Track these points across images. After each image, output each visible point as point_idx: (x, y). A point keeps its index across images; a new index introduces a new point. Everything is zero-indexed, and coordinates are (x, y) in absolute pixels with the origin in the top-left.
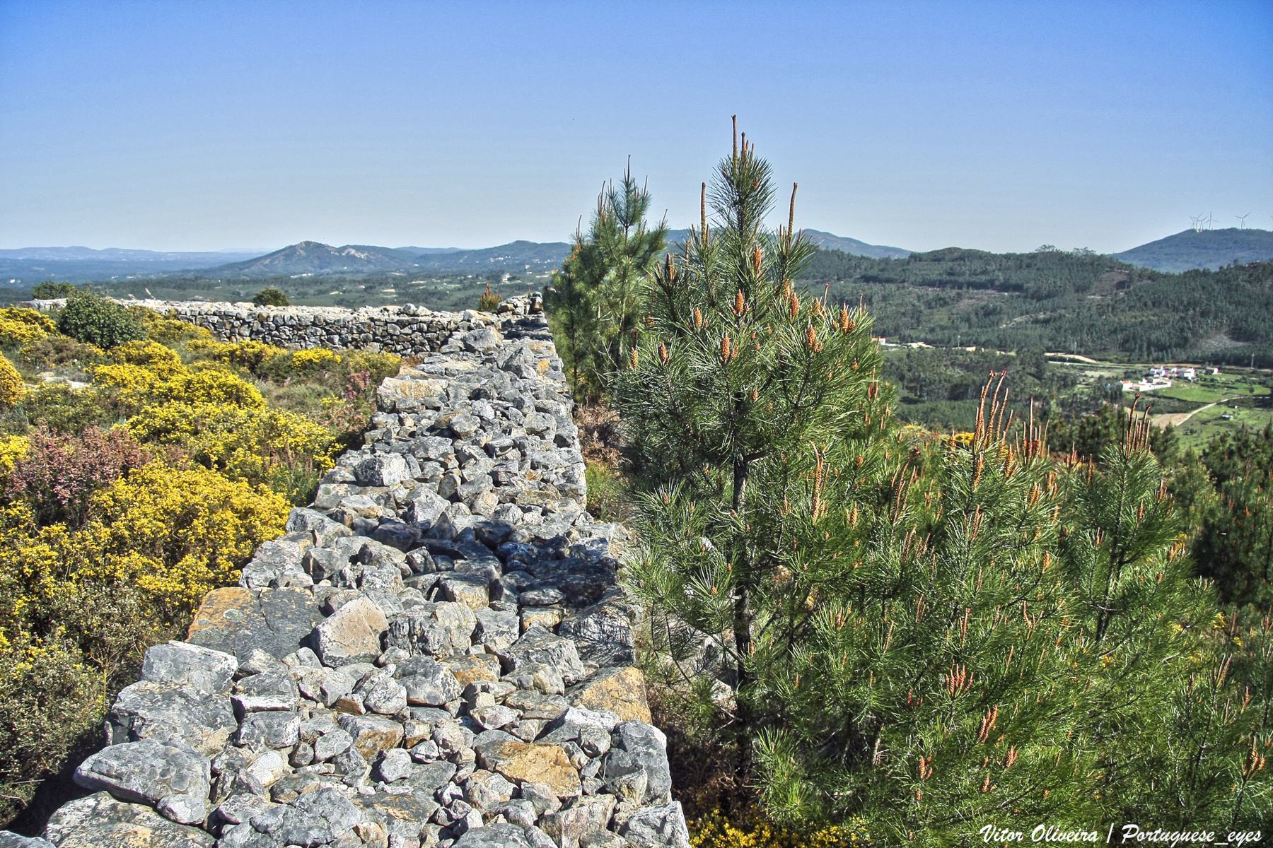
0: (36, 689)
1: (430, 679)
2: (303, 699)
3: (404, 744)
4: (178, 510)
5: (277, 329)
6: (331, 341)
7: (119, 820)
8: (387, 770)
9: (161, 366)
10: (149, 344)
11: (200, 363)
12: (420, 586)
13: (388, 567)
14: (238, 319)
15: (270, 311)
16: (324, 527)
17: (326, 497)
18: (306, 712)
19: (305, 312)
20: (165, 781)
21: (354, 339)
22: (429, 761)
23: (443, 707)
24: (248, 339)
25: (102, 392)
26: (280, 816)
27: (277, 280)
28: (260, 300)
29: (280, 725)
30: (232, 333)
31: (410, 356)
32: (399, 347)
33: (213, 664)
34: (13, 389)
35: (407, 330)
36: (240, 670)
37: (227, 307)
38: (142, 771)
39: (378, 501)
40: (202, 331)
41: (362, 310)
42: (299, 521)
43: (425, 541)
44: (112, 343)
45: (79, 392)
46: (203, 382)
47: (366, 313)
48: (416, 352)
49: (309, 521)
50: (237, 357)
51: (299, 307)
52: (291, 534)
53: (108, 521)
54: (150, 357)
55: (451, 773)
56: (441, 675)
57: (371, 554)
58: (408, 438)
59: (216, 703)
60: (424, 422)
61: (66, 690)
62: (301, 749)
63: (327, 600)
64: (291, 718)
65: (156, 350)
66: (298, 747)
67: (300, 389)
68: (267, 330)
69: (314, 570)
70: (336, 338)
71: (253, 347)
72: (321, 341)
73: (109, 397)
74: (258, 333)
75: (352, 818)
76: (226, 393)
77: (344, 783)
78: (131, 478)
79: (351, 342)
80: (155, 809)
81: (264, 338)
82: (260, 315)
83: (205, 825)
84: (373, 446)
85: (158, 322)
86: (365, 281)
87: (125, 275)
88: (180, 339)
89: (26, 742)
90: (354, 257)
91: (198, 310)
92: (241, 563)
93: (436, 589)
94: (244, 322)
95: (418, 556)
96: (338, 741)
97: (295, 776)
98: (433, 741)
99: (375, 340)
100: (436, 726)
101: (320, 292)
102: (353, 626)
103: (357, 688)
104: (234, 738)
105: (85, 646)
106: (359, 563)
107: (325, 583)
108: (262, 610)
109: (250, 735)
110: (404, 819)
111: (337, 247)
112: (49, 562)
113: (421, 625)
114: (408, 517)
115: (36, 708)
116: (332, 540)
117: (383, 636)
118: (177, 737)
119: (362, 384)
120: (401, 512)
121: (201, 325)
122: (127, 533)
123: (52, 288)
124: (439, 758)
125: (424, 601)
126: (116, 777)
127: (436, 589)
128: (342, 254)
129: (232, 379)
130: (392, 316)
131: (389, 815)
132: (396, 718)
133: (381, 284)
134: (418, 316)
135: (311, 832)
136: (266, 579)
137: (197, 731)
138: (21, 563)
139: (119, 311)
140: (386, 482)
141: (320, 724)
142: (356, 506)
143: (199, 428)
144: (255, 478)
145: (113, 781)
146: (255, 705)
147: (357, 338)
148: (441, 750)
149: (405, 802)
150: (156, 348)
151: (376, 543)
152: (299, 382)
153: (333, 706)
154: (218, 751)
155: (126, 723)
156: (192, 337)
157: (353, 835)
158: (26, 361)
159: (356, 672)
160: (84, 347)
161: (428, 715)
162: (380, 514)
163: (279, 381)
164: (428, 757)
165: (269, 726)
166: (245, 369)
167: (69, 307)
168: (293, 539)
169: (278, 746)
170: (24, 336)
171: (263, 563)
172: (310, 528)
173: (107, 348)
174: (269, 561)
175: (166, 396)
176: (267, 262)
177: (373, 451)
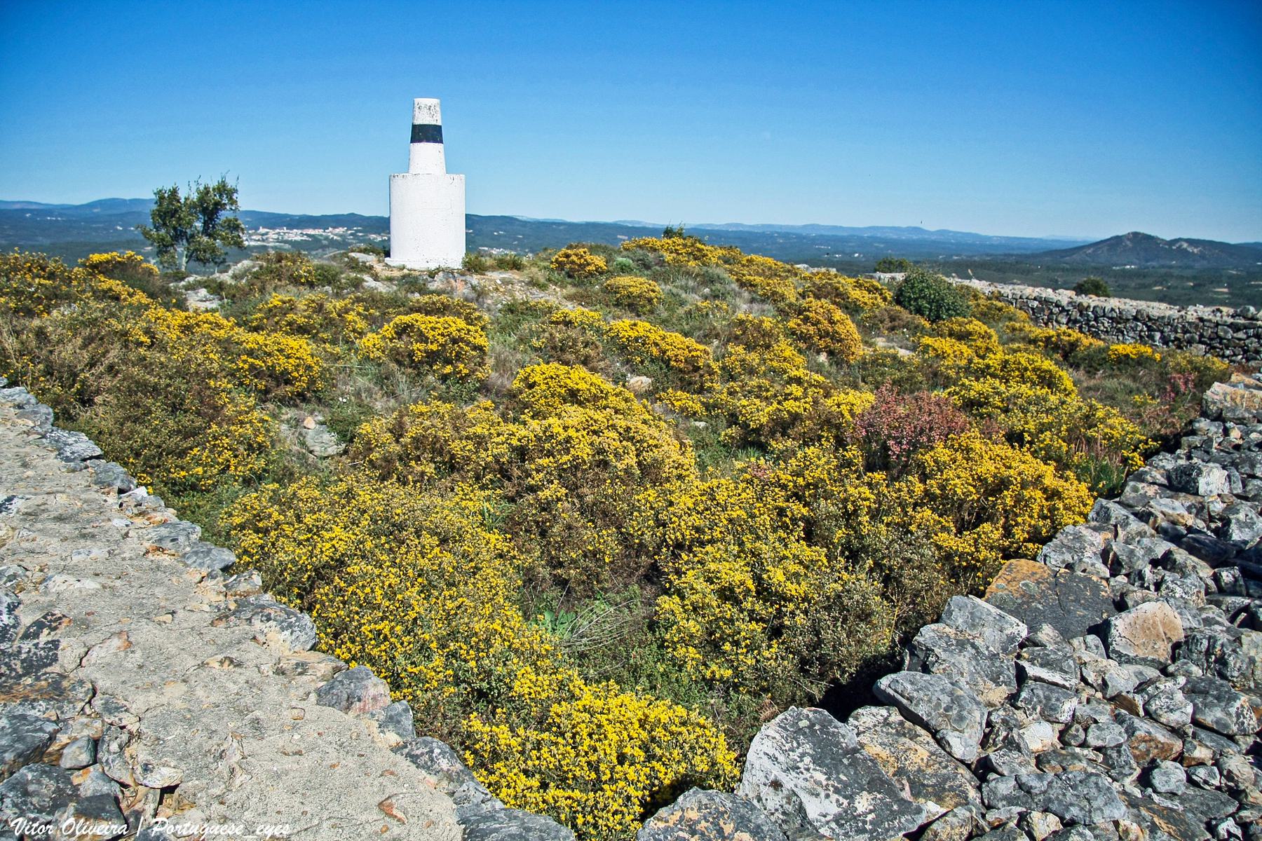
0: (843, 608)
1: (1223, 704)
2: (1083, 684)
3: (1180, 759)
4: (990, 480)
5: (1096, 319)
6: (1151, 337)
7: (904, 735)
8: (1158, 779)
9: (979, 344)
10: (971, 322)
11: (1016, 346)
12: (1224, 607)
13: (1192, 580)
14: (1057, 306)
15: (1091, 301)
16: (1128, 524)
17: (1133, 495)
18: (1084, 696)
19: (1129, 306)
20: (946, 716)
21: (1176, 339)
22: (1207, 787)
23: (1231, 738)
24: (1064, 328)
25: (925, 361)
26: (1045, 783)
27: (1096, 270)
28: (1080, 290)
29: (1058, 700)
30: (1050, 320)
31: (1240, 363)
32: (1228, 352)
33: (1006, 626)
34: (853, 349)
35: (1241, 335)
36: (1028, 639)
37: (1048, 293)
38: (929, 701)
39: (1189, 509)
40: (1021, 315)
41: (1191, 308)
42: (1102, 513)
43: (1239, 562)
44: (938, 317)
45: (906, 359)
46: (1020, 363)
47: (1195, 312)
48: (1248, 360)
49: (1113, 515)
50: (1052, 343)
51: (1123, 300)
52: (1093, 524)
53: (924, 478)
54: (970, 334)
55: (1231, 810)
56: (1238, 704)
57: (1175, 561)
58: (1232, 451)
59: (1002, 662)
60: (1253, 436)
61: (865, 616)
62: (1073, 729)
63: (1123, 595)
64: (1068, 697)
65: (976, 328)
66: (1071, 726)
67: (1112, 383)
68: (1084, 319)
69: (1112, 561)
70: (1158, 335)
71: (1069, 335)
72: (1141, 337)
73: (931, 367)
74: (1075, 321)
75: (1115, 811)
76: (1039, 377)
77: (1110, 776)
78: (949, 443)
79: (1173, 341)
80: (934, 736)
81: (1080, 328)
82: (1080, 304)
83: (973, 766)
84: (1190, 452)
85: (981, 302)
86: (1194, 278)
87: (952, 256)
88: (999, 320)
89: (826, 649)
90: (1185, 250)
91: (1019, 293)
92: (1038, 538)
93: (1243, 615)
94: (1063, 310)
95: (1227, 576)
96: (1113, 735)
97: (1063, 752)
98: (1215, 769)
99: (1201, 342)
100: (1221, 755)
101: (1144, 286)
102: (1147, 628)
103: (1140, 689)
104: (1013, 699)
105: (887, 580)
106: (1160, 568)
107: (1121, 579)
108: (1057, 589)
109: (1026, 701)
110: (1170, 833)
111: (1168, 239)
112: (867, 503)
113: (1222, 645)
114: (1222, 533)
115: (839, 624)
116: (1133, 539)
117: (1176, 646)
118: (963, 681)
119: (1182, 388)
120: (1213, 526)
121: (1020, 309)
122: (938, 492)
123: (891, 263)
124: (1219, 788)
125: (1227, 624)
126: (908, 699)
127: (1243, 615)
128: (1172, 248)
129: (1048, 365)
130: (1225, 318)
131: (1153, 823)
132: (1176, 731)
133: (1212, 282)
134: (1257, 320)
135: (1071, 808)
136: (1063, 562)
137: (981, 682)
138: (845, 500)
139: (948, 288)
140: (1201, 491)
141: (1096, 712)
142: (1164, 509)
143: (1010, 406)
144: (1062, 466)
145: (905, 701)
146: (1038, 675)
147: (1180, 337)
148: (1224, 781)
149: (1173, 817)
150: (977, 326)
151: (1181, 551)
152: (1112, 376)
153: (1111, 699)
154: (995, 706)
155: (922, 656)
156: (1010, 319)
157: (1111, 827)
158: (865, 326)
159: (1141, 673)
160: (914, 319)
161: (1212, 741)
162: (1190, 523)
163: (1091, 372)
164: (1206, 782)
165: (1048, 698)
166: (1058, 356)
167: (906, 281)
168: (1095, 529)
169: (1051, 719)
170: (865, 304)
171: (1063, 545)
172: (1113, 521)
173: (933, 322)
174: (1069, 544)
175: (983, 372)
176: (1090, 251)
177: (1189, 457)
